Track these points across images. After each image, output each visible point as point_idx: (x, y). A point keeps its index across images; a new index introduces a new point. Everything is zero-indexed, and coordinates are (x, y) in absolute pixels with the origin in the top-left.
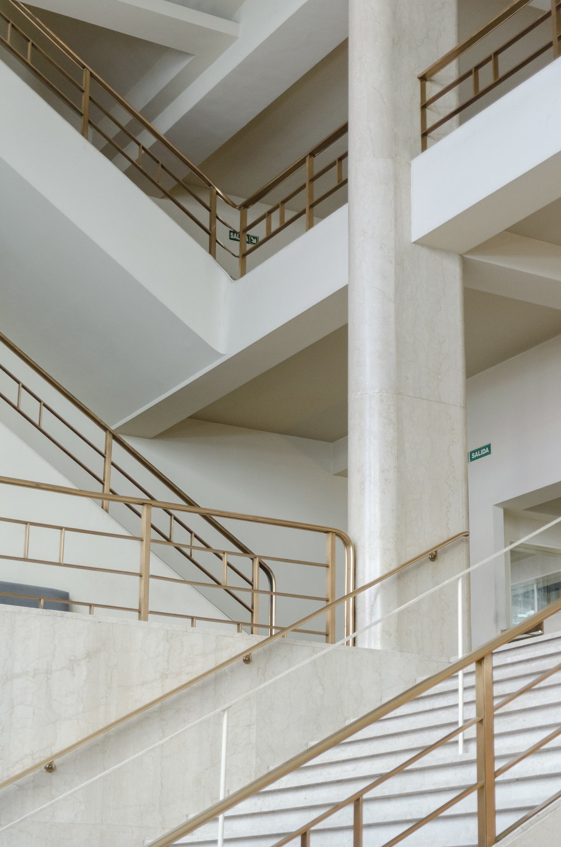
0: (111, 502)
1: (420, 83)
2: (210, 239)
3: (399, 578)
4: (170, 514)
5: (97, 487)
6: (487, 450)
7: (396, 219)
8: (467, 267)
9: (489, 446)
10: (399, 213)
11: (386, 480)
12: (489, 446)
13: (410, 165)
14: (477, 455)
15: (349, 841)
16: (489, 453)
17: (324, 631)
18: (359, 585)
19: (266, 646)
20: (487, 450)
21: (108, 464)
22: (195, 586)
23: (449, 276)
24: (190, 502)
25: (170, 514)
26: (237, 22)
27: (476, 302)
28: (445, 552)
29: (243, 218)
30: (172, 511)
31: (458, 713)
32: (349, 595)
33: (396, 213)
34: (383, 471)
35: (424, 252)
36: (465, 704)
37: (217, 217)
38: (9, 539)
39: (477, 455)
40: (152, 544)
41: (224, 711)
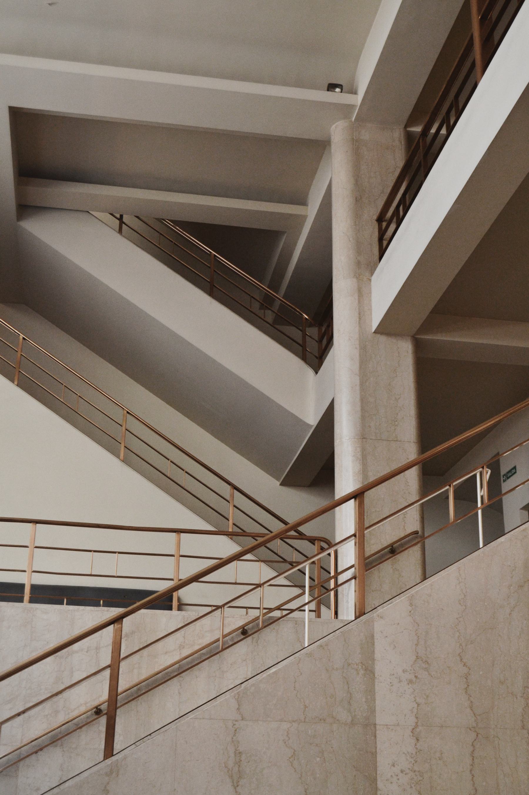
1: (377, 224)
6: (514, 471)
7: (360, 319)
8: (419, 347)
9: (515, 468)
10: (362, 314)
12: (515, 468)
13: (370, 280)
14: (510, 474)
15: (199, 645)
16: (515, 472)
18: (340, 570)
20: (514, 471)
21: (231, 508)
26: (328, 90)
27: (429, 370)
29: (320, 331)
31: (305, 614)
32: (333, 577)
33: (359, 314)
35: (383, 339)
36: (310, 611)
39: (510, 474)
40: (181, 558)
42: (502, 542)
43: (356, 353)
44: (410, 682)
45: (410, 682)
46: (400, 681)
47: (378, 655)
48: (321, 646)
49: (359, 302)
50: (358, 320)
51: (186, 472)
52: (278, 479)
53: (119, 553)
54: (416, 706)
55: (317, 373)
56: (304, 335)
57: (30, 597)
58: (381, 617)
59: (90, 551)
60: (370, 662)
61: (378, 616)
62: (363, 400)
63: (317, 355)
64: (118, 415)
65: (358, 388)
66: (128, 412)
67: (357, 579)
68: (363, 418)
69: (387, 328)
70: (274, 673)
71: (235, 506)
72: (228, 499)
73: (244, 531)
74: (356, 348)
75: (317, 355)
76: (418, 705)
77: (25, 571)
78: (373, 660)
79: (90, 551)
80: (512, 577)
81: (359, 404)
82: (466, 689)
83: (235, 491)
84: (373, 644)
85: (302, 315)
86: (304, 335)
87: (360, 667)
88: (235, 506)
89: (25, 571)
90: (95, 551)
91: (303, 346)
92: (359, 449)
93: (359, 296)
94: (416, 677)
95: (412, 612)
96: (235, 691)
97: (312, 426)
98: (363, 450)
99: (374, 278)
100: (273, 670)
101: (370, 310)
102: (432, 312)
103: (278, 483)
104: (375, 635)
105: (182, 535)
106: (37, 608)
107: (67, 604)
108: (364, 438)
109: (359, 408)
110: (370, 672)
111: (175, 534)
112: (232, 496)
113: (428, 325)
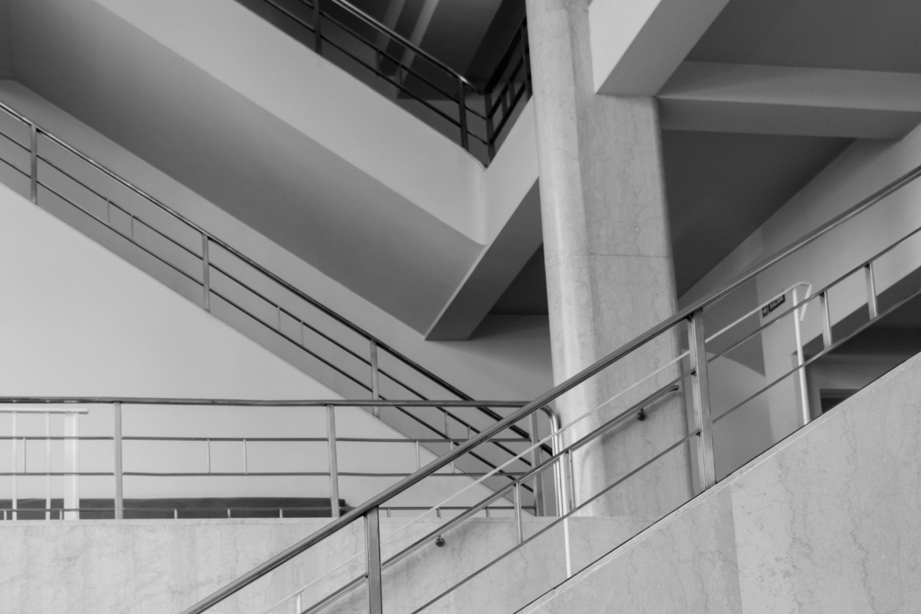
0: (382, 408)
2: (462, 131)
3: (604, 441)
4: (444, 411)
5: (364, 395)
7: (575, 73)
8: (663, 110)
10: (578, 65)
11: (582, 345)
13: (587, 11)
17: (533, 505)
19: (459, 525)
21: (375, 372)
22: (410, 478)
23: (642, 121)
24: (465, 397)
25: (444, 411)
28: (655, 408)
29: (488, 101)
30: (445, 408)
34: (579, 336)
37: (466, 108)
38: (11, 456)
40: (337, 442)
41: (297, 595)
42: (902, 373)
43: (573, 125)
44: (787, 574)
45: (787, 574)
46: (773, 574)
47: (739, 539)
48: (661, 530)
49: (572, 46)
50: (572, 74)
51: (305, 324)
52: (422, 332)
53: (248, 440)
54: (797, 606)
55: (486, 166)
56: (463, 109)
57: (124, 511)
58: (741, 486)
59: (205, 439)
60: (730, 550)
61: (736, 484)
62: (587, 197)
63: (486, 139)
64: (195, 242)
65: (578, 178)
66: (209, 238)
67: (702, 434)
68: (588, 224)
69: (618, 87)
70: (599, 571)
71: (379, 370)
72: (368, 359)
73: (425, 399)
74: (572, 118)
75: (486, 139)
76: (800, 605)
77: (112, 474)
78: (734, 546)
79: (205, 439)
80: (918, 422)
81: (581, 203)
82: (864, 580)
83: (379, 349)
84: (732, 524)
85: (457, 77)
86: (463, 109)
87: (717, 557)
88: (379, 370)
89: (112, 474)
90: (212, 439)
91: (462, 125)
92: (584, 271)
93: (571, 38)
94: (794, 567)
95: (783, 476)
96: (548, 599)
97: (483, 246)
98: (591, 270)
99: (592, 8)
100: (596, 567)
101: (589, 57)
102: (688, 58)
103: (423, 337)
104: (734, 511)
105: (336, 408)
106: (138, 526)
107: (179, 517)
108: (592, 254)
109: (581, 209)
110: (730, 563)
111: (325, 408)
112: (374, 355)
113: (676, 81)
